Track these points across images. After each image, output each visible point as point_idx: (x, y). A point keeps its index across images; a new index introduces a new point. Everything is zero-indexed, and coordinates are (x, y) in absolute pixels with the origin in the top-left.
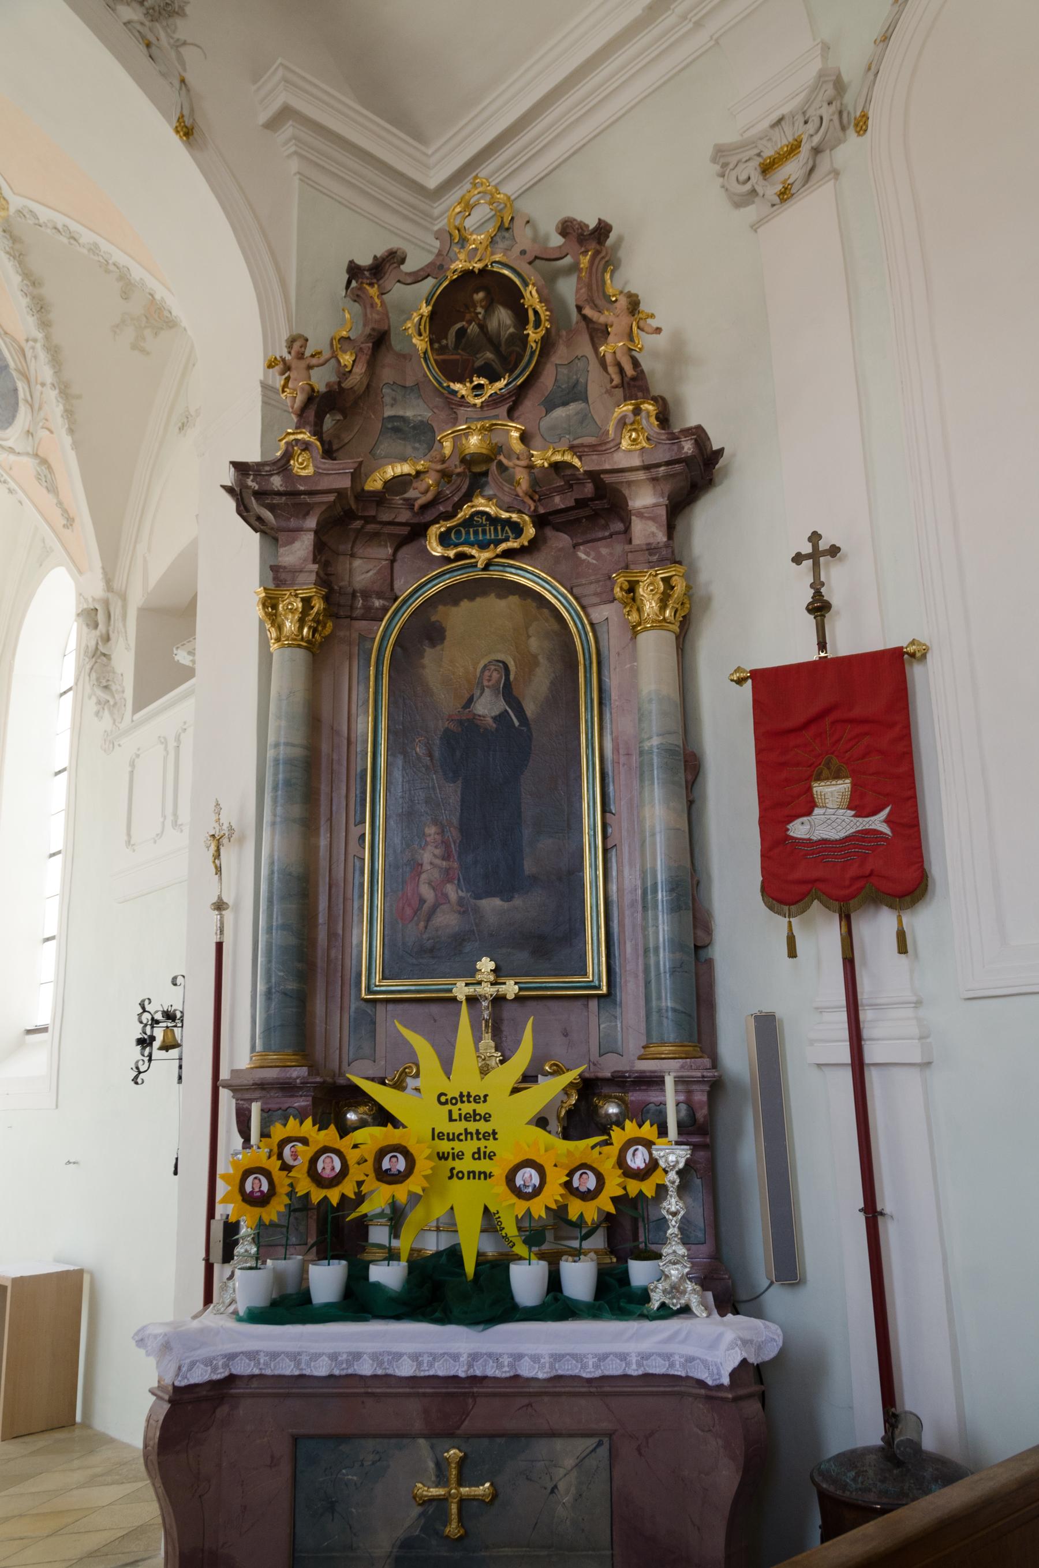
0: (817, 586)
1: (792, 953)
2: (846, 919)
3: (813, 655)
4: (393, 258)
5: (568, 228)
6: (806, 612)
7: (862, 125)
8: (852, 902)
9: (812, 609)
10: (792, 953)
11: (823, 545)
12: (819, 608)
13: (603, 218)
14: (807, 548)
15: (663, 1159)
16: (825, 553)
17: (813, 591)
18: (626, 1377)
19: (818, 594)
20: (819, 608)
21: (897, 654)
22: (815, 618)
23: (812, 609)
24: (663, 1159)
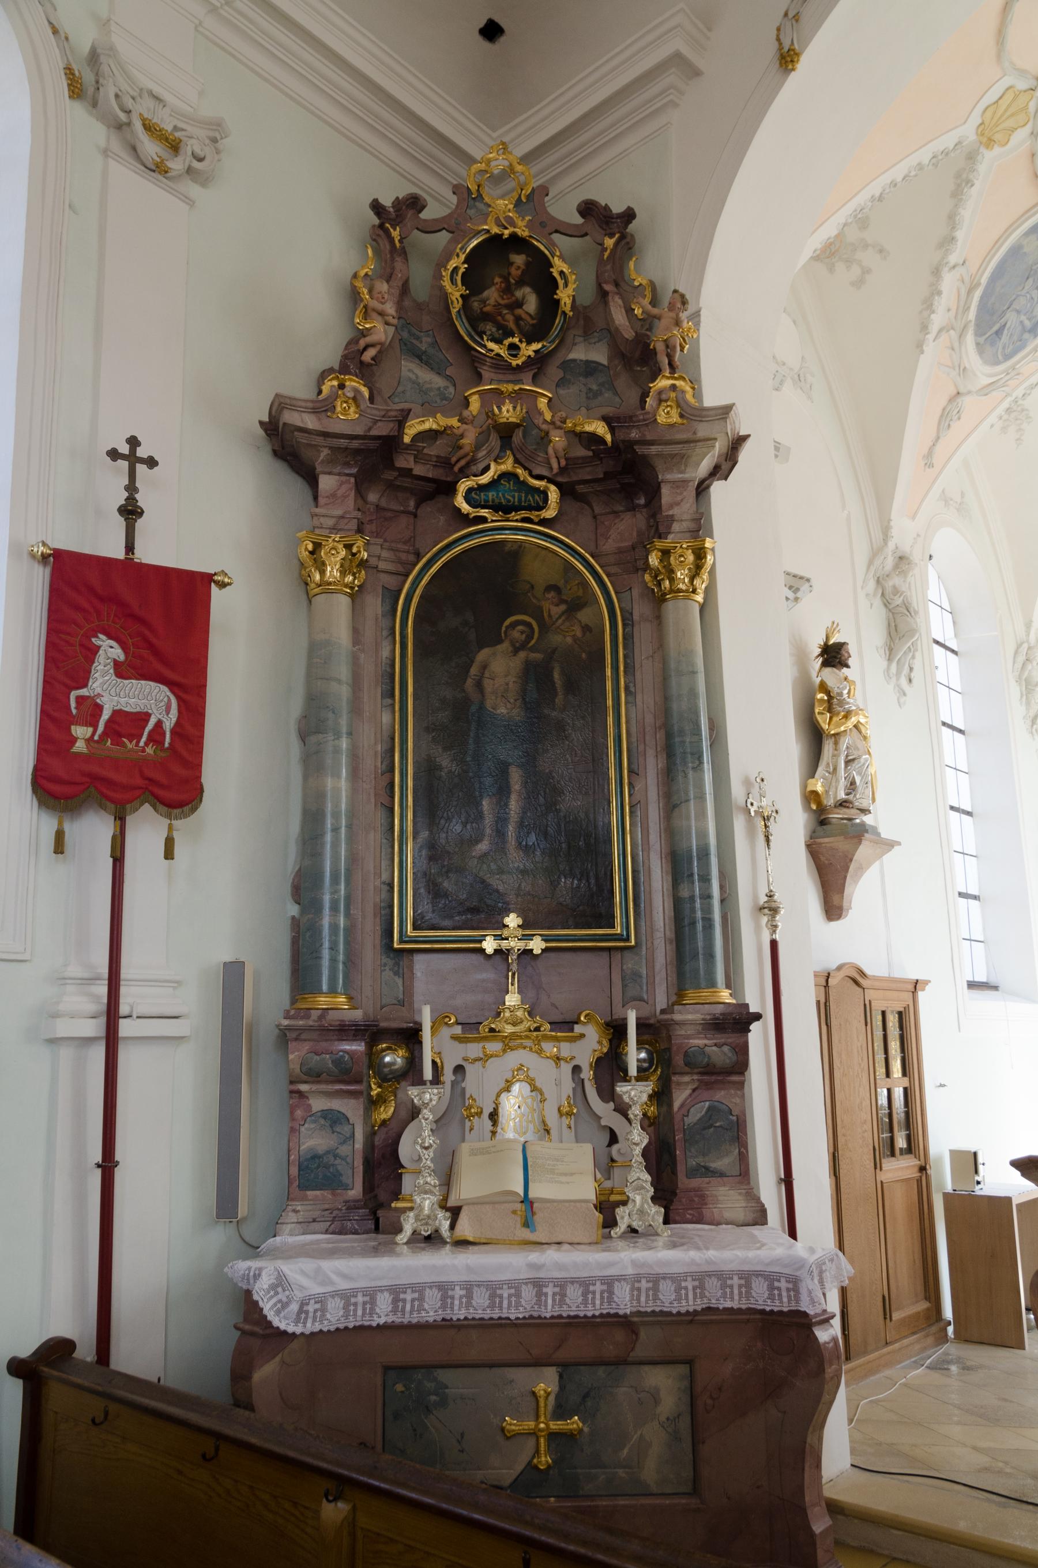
0: (131, 488)
1: (169, 854)
2: (121, 819)
3: (120, 554)
4: (414, 203)
5: (588, 209)
6: (117, 514)
7: (919, 164)
8: (128, 806)
9: (124, 510)
10: (169, 854)
11: (124, 449)
12: (131, 512)
13: (609, 204)
14: (142, 452)
15: (627, 1095)
16: (142, 461)
17: (126, 494)
18: (781, 1312)
19: (131, 500)
20: (131, 512)
21: (207, 579)
22: (125, 520)
23: (124, 510)
24: (627, 1095)
